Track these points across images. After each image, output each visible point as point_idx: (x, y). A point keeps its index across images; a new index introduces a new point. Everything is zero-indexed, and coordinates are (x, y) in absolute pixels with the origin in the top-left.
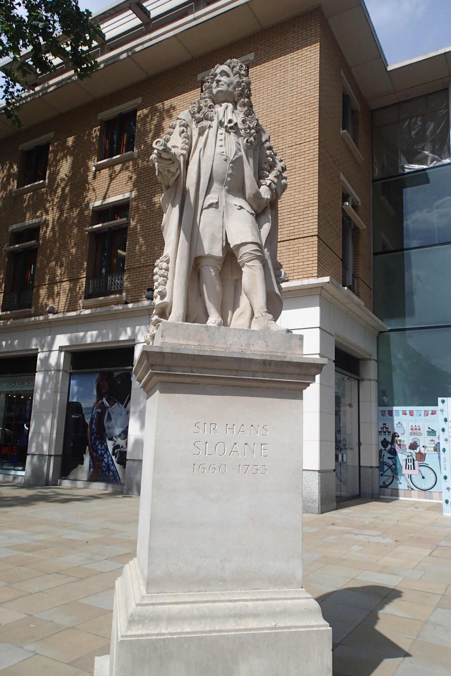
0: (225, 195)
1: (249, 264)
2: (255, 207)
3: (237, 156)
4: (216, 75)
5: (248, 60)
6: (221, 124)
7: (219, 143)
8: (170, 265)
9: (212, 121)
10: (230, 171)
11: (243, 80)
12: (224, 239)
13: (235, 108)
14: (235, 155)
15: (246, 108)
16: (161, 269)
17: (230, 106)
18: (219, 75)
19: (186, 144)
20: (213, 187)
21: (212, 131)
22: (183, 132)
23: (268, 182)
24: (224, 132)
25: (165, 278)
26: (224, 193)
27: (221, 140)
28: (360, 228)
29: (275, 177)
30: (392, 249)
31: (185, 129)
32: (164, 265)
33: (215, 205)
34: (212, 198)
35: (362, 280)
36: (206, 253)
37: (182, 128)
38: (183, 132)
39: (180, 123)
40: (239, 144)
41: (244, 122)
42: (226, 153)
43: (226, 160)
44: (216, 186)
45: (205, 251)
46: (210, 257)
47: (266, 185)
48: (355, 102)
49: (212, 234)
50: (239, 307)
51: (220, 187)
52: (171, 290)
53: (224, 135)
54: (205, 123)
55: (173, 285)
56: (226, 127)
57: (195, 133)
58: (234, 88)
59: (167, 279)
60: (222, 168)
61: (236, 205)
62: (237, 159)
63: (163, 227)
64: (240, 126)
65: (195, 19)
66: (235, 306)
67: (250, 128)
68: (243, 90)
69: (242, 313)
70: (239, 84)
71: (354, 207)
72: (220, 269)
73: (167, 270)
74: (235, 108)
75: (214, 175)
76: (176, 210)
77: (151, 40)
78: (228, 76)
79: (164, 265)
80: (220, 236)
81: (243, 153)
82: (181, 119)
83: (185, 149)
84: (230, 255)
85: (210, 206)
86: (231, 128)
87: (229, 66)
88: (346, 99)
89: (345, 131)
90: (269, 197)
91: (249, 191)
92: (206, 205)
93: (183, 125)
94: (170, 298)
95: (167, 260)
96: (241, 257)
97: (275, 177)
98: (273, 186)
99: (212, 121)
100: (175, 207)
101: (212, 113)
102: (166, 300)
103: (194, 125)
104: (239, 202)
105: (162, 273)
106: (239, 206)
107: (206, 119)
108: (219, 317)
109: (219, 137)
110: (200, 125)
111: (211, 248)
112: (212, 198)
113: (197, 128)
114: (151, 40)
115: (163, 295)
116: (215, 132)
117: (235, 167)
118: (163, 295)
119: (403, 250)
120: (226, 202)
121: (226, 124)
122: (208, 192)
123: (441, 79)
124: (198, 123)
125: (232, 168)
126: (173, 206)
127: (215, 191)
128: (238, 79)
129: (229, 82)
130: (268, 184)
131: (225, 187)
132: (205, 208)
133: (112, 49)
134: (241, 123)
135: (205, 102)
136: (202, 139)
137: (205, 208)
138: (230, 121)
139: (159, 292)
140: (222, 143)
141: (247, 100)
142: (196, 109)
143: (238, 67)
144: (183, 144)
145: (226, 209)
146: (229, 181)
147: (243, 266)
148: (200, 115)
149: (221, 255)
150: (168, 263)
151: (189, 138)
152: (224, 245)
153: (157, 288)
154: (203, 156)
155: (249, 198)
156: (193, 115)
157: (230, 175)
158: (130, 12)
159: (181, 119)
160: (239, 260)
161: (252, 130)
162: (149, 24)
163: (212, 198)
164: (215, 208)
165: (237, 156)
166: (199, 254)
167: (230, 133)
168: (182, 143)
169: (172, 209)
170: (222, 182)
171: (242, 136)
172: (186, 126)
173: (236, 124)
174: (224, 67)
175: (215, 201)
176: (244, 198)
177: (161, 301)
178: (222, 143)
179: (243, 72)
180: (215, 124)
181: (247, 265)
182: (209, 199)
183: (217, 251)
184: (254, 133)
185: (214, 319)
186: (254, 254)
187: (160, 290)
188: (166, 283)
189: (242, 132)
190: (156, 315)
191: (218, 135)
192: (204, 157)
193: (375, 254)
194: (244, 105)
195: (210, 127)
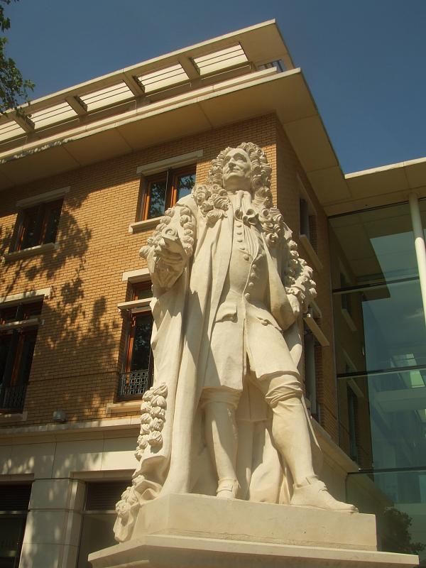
0: (246, 305)
1: (284, 403)
2: (282, 323)
3: (260, 255)
4: (228, 158)
5: (196, 157)
6: (238, 214)
7: (237, 238)
8: (168, 400)
9: (225, 211)
10: (252, 274)
11: (263, 166)
12: (245, 364)
13: (253, 198)
14: (259, 253)
15: (266, 199)
16: (155, 405)
17: (247, 194)
18: (232, 159)
19: (191, 236)
20: (230, 293)
21: (226, 223)
22: (187, 221)
23: (296, 291)
24: (242, 224)
25: (160, 420)
26: (243, 301)
27: (241, 234)
28: (323, 345)
29: (302, 284)
30: (356, 370)
31: (189, 217)
32: (160, 399)
33: (233, 318)
34: (228, 308)
35: (326, 407)
36: (222, 384)
37: (185, 217)
38: (187, 221)
39: (181, 210)
40: (262, 241)
41: (266, 214)
42: (247, 250)
43: (247, 259)
44: (232, 292)
45: (221, 381)
46: (226, 390)
47: (293, 293)
48: (312, 208)
49: (229, 358)
50: (262, 462)
51: (239, 294)
52: (169, 438)
53: (242, 227)
54: (215, 212)
55: (172, 430)
56: (245, 218)
57: (202, 223)
58: (252, 174)
59: (164, 420)
60: (242, 270)
61: (261, 319)
62: (261, 257)
63: (155, 344)
64: (261, 219)
65: (137, 115)
66: (256, 460)
67: (272, 221)
68: (262, 178)
69: (265, 474)
70: (258, 170)
71: (316, 319)
72: (236, 406)
73: (164, 407)
74: (253, 198)
75: (231, 278)
76: (178, 319)
77: (86, 131)
78: (244, 160)
79: (160, 399)
80: (239, 360)
81: (266, 251)
82: (183, 206)
83: (189, 242)
84: (254, 387)
85: (226, 318)
86: (251, 220)
87: (245, 150)
88: (303, 204)
89: (304, 235)
90: (298, 310)
91: (275, 300)
92: (219, 317)
93: (187, 213)
94: (167, 451)
95: (165, 392)
96: (273, 392)
97: (302, 284)
98: (303, 296)
99: (225, 211)
100: (176, 316)
101: (225, 200)
102: (162, 453)
103: (199, 213)
104: (263, 314)
105: (156, 412)
106: (265, 321)
107: (217, 208)
108: (235, 481)
109: (237, 230)
110: (210, 214)
111: (227, 378)
112: (228, 308)
113: (205, 217)
114: (86, 131)
115: (156, 446)
116: (231, 223)
117: (258, 269)
118: (156, 446)
119: (366, 373)
120: (246, 314)
121: (245, 215)
122: (222, 300)
123: (398, 191)
124: (207, 211)
125: (255, 269)
126: (173, 314)
127: (230, 299)
128: (256, 165)
129: (245, 167)
130: (296, 293)
131: (245, 293)
132: (219, 321)
133: (40, 138)
134: (263, 215)
135: (214, 188)
136: (213, 232)
137: (219, 321)
138: (250, 212)
139: (151, 442)
140: (241, 237)
141: (267, 189)
142: (204, 195)
143: (256, 152)
144: (187, 236)
145: (247, 324)
146: (251, 286)
147: (275, 406)
148: (210, 202)
149: (241, 388)
150: (165, 397)
151: (195, 228)
152: (245, 374)
153: (146, 433)
154: (215, 252)
155: (275, 310)
156: (199, 202)
157: (252, 279)
158: (66, 104)
159: (183, 206)
160: (269, 395)
161: (276, 225)
162: (85, 116)
163: (228, 308)
164: (233, 321)
165: (260, 255)
166: (208, 385)
167: (249, 227)
168: (185, 235)
169: (169, 319)
170: (241, 287)
171: (263, 231)
172: (190, 213)
173: (257, 216)
174: (239, 150)
175: (233, 312)
176: (268, 309)
177: (153, 455)
178: (241, 237)
179: (261, 157)
180: (230, 213)
181: (282, 405)
182: (224, 309)
183: (235, 381)
184: (278, 228)
185: (227, 484)
186: (293, 390)
187: (154, 438)
188: (162, 426)
189: (264, 226)
190: (141, 474)
191: (235, 227)
192: (216, 254)
193: (339, 376)
194: (264, 194)
195: (223, 217)
